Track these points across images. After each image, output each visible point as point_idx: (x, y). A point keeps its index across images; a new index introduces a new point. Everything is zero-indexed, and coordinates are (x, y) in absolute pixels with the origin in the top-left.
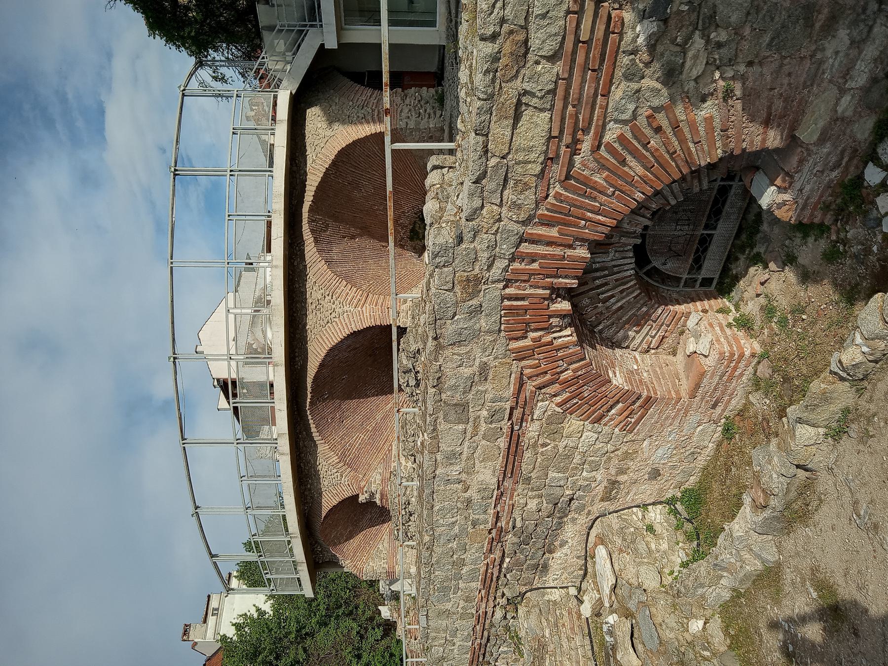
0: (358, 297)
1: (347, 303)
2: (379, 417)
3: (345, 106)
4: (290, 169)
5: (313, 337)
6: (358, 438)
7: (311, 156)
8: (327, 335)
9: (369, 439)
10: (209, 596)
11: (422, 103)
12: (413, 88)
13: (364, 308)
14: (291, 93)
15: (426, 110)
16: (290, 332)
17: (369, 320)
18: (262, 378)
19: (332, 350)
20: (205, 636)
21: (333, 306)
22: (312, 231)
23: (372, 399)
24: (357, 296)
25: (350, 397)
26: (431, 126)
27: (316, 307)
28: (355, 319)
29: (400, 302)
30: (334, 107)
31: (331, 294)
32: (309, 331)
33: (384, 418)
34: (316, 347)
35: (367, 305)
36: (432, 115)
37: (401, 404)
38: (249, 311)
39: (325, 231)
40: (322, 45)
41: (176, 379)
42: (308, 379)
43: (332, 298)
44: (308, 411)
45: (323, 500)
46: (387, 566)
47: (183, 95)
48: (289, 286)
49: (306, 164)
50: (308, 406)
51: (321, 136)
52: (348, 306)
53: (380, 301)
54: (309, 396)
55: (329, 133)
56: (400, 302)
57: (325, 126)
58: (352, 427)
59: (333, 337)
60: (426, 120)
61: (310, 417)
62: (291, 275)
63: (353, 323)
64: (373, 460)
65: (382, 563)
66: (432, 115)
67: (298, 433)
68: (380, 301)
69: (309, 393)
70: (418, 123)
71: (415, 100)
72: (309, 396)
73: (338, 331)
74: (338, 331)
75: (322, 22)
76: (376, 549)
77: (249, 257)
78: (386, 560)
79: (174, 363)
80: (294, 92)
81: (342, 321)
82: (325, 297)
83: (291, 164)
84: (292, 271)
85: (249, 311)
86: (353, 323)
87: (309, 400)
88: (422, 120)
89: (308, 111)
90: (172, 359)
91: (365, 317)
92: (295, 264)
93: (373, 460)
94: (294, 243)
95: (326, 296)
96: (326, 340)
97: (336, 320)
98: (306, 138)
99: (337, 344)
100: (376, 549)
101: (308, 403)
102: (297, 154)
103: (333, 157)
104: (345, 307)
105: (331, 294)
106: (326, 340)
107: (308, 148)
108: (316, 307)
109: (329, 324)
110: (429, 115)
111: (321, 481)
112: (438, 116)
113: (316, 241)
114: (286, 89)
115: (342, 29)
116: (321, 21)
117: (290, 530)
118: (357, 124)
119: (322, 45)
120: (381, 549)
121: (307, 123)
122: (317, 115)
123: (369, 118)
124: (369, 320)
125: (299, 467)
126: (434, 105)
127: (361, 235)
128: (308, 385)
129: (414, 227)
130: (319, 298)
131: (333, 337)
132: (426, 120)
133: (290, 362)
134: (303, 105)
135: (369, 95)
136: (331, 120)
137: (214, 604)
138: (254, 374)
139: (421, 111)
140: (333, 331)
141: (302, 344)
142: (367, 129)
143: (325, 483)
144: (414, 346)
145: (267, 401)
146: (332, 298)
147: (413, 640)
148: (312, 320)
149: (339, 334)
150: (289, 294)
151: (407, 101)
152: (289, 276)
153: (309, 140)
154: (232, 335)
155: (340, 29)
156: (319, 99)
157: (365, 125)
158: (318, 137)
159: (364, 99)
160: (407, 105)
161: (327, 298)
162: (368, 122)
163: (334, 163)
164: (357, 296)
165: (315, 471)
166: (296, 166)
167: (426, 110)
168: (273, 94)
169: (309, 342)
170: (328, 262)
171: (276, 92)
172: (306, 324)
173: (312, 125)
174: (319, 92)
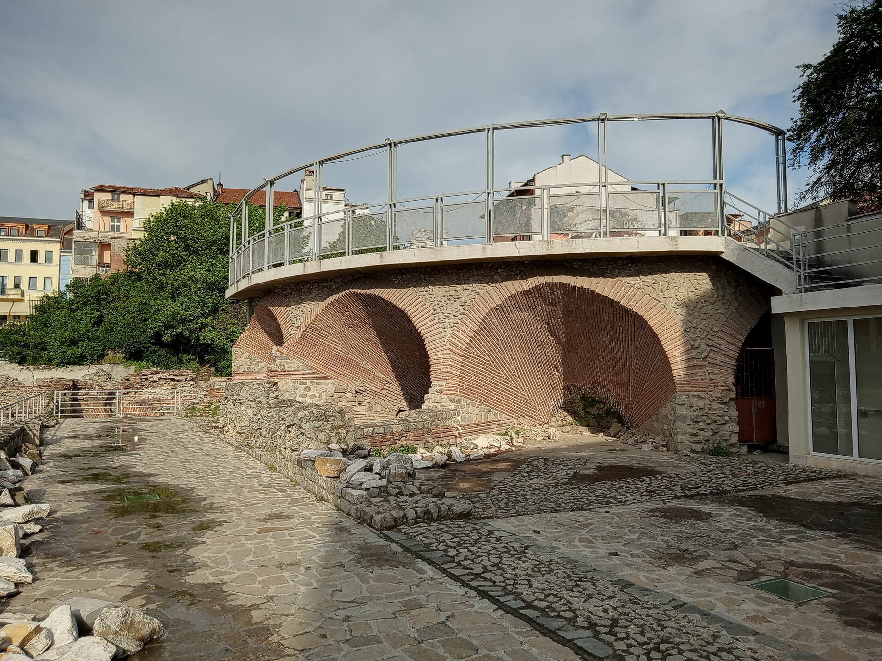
0: (460, 345)
1: (455, 332)
2: (366, 364)
3: (713, 322)
4: (620, 258)
5: (421, 294)
6: (337, 345)
7: (639, 281)
8: (421, 309)
9: (337, 355)
10: (343, 190)
11: (714, 426)
12: (737, 413)
13: (448, 351)
14: (722, 252)
15: (703, 430)
16: (426, 268)
17: (435, 357)
18: (535, 227)
19: (403, 314)
20: (308, 190)
21: (451, 316)
22: (537, 288)
23: (385, 357)
24: (461, 343)
25: (380, 333)
26: (679, 437)
27: (452, 296)
28: (437, 341)
29: (451, 394)
30: (710, 307)
31: (465, 312)
32: (427, 289)
33: (367, 372)
34: (410, 298)
35: (451, 355)
36: (694, 439)
37: (386, 388)
38: (604, 205)
39: (545, 302)
40: (777, 292)
41: (371, 148)
42: (379, 290)
43: (460, 314)
44: (348, 291)
45: (282, 308)
46: (241, 371)
47: (716, 120)
48: (475, 264)
49: (628, 276)
50: (354, 290)
51: (666, 292)
52: (451, 333)
53: (453, 370)
54: (363, 292)
55: (671, 303)
56: (451, 394)
57: (681, 297)
58: (346, 336)
59: (419, 316)
60: (689, 430)
61: (344, 293)
62: (487, 266)
63: (433, 338)
64: (314, 360)
65: (244, 366)
66: (694, 439)
67: (334, 279)
68: (453, 370)
69: (365, 291)
70: (683, 418)
71: (718, 416)
72: (363, 292)
73: (424, 322)
74: (424, 322)
75: (805, 292)
76: (260, 360)
77: (672, 200)
78: (247, 370)
79: (386, 145)
80: (723, 256)
81: (435, 326)
82: (462, 306)
83: (626, 258)
84: (492, 267)
85: (604, 205)
86: (433, 338)
87: (359, 291)
88: (688, 425)
89: (705, 275)
90: (388, 142)
91: (440, 353)
92: (500, 270)
93: (314, 360)
94: (525, 267)
95: (463, 307)
96: (415, 309)
97: (436, 320)
98: (663, 275)
99: (410, 321)
100: (260, 360)
101: (356, 291)
102: (640, 265)
103: (635, 310)
104: (450, 329)
105: (465, 312)
106: (415, 309)
107: (650, 277)
108: (452, 296)
109: (432, 311)
110: (695, 435)
111: (296, 306)
112: (695, 446)
113: (526, 293)
114: (727, 245)
115: (802, 321)
116: (807, 290)
117: (579, 241)
118: (683, 338)
119: (777, 292)
120: (260, 364)
121: (685, 274)
122: (698, 287)
123: (694, 354)
124: (435, 357)
125: (308, 282)
126: (711, 441)
127: (559, 342)
128: (373, 290)
129: (599, 402)
130: (461, 299)
131: (419, 316)
132: (689, 430)
133: (398, 269)
134: (714, 267)
135: (729, 354)
136: (692, 307)
137: (337, 195)
138: (540, 218)
139: (701, 424)
140: (425, 316)
141: (414, 282)
142: (676, 353)
143: (293, 310)
144: (307, 428)
145: (350, 248)
146: (460, 314)
147: (204, 393)
148: (437, 292)
149: (421, 323)
150: (466, 264)
151: (716, 405)
152: (485, 263)
153: (661, 279)
154: (583, 190)
155: (801, 316)
156: (723, 288)
157: (682, 349)
158: (664, 289)
159: (723, 347)
160: (710, 405)
161: (462, 308)
162: (687, 352)
163: (628, 312)
164: (461, 343)
165: (304, 299)
166: (624, 265)
167: (703, 430)
168: (720, 229)
169: (415, 289)
170: (500, 308)
171: (723, 234)
172: (433, 284)
173: (682, 281)
174: (736, 288)
